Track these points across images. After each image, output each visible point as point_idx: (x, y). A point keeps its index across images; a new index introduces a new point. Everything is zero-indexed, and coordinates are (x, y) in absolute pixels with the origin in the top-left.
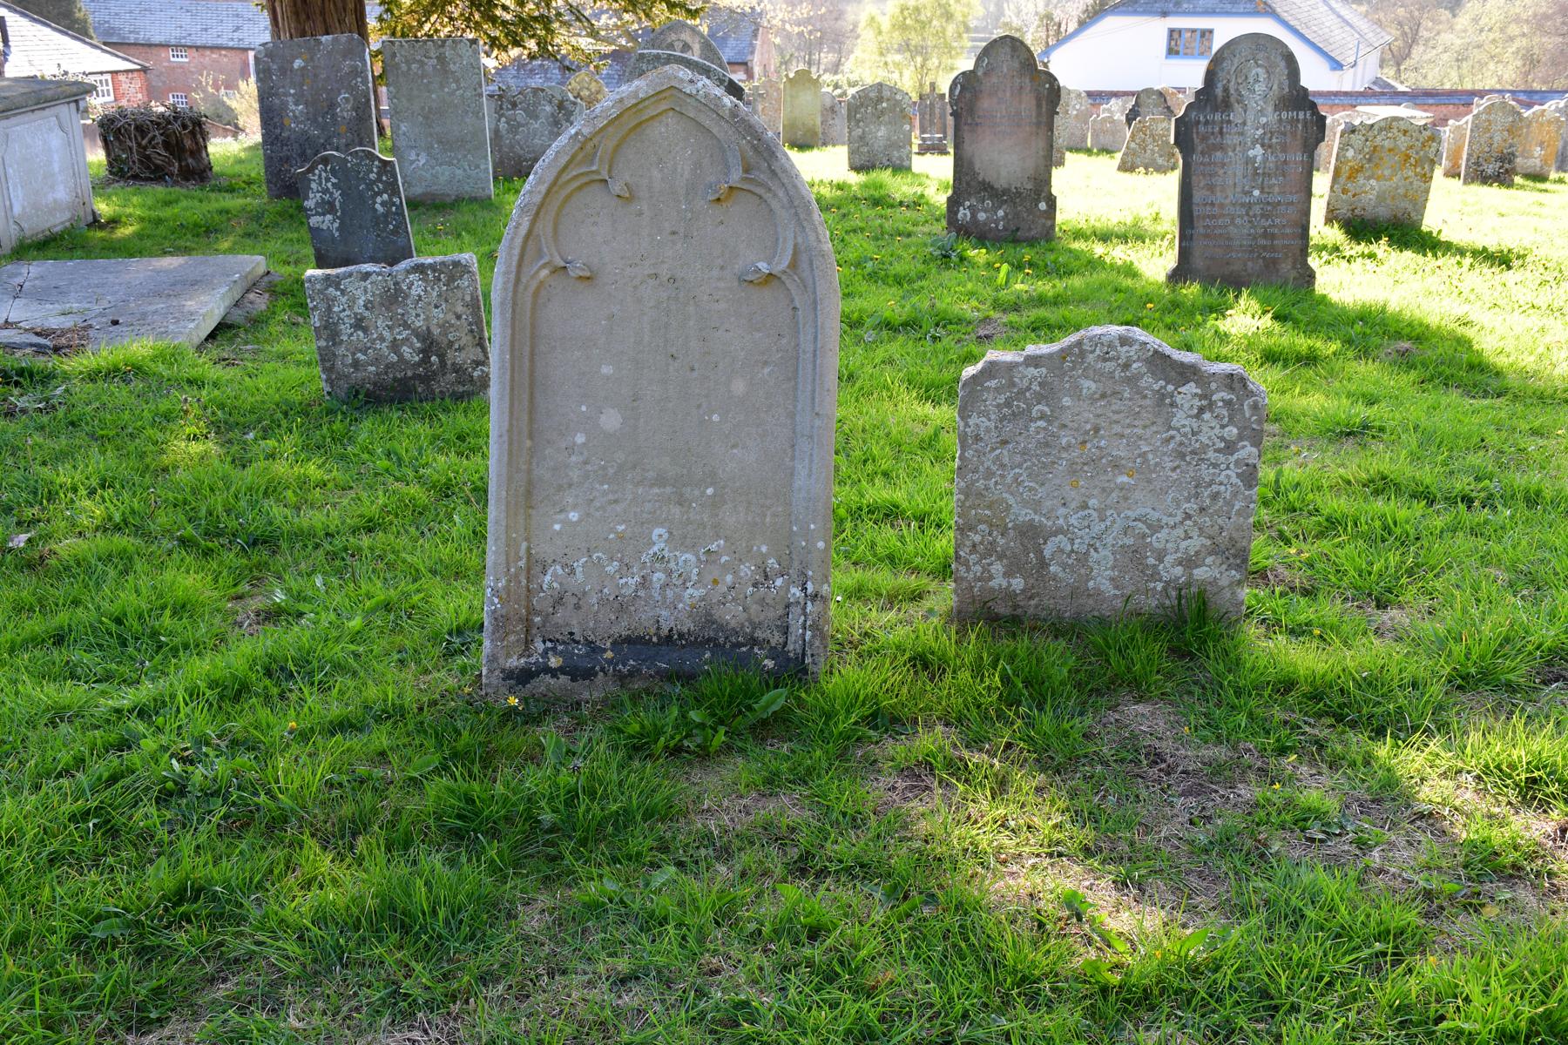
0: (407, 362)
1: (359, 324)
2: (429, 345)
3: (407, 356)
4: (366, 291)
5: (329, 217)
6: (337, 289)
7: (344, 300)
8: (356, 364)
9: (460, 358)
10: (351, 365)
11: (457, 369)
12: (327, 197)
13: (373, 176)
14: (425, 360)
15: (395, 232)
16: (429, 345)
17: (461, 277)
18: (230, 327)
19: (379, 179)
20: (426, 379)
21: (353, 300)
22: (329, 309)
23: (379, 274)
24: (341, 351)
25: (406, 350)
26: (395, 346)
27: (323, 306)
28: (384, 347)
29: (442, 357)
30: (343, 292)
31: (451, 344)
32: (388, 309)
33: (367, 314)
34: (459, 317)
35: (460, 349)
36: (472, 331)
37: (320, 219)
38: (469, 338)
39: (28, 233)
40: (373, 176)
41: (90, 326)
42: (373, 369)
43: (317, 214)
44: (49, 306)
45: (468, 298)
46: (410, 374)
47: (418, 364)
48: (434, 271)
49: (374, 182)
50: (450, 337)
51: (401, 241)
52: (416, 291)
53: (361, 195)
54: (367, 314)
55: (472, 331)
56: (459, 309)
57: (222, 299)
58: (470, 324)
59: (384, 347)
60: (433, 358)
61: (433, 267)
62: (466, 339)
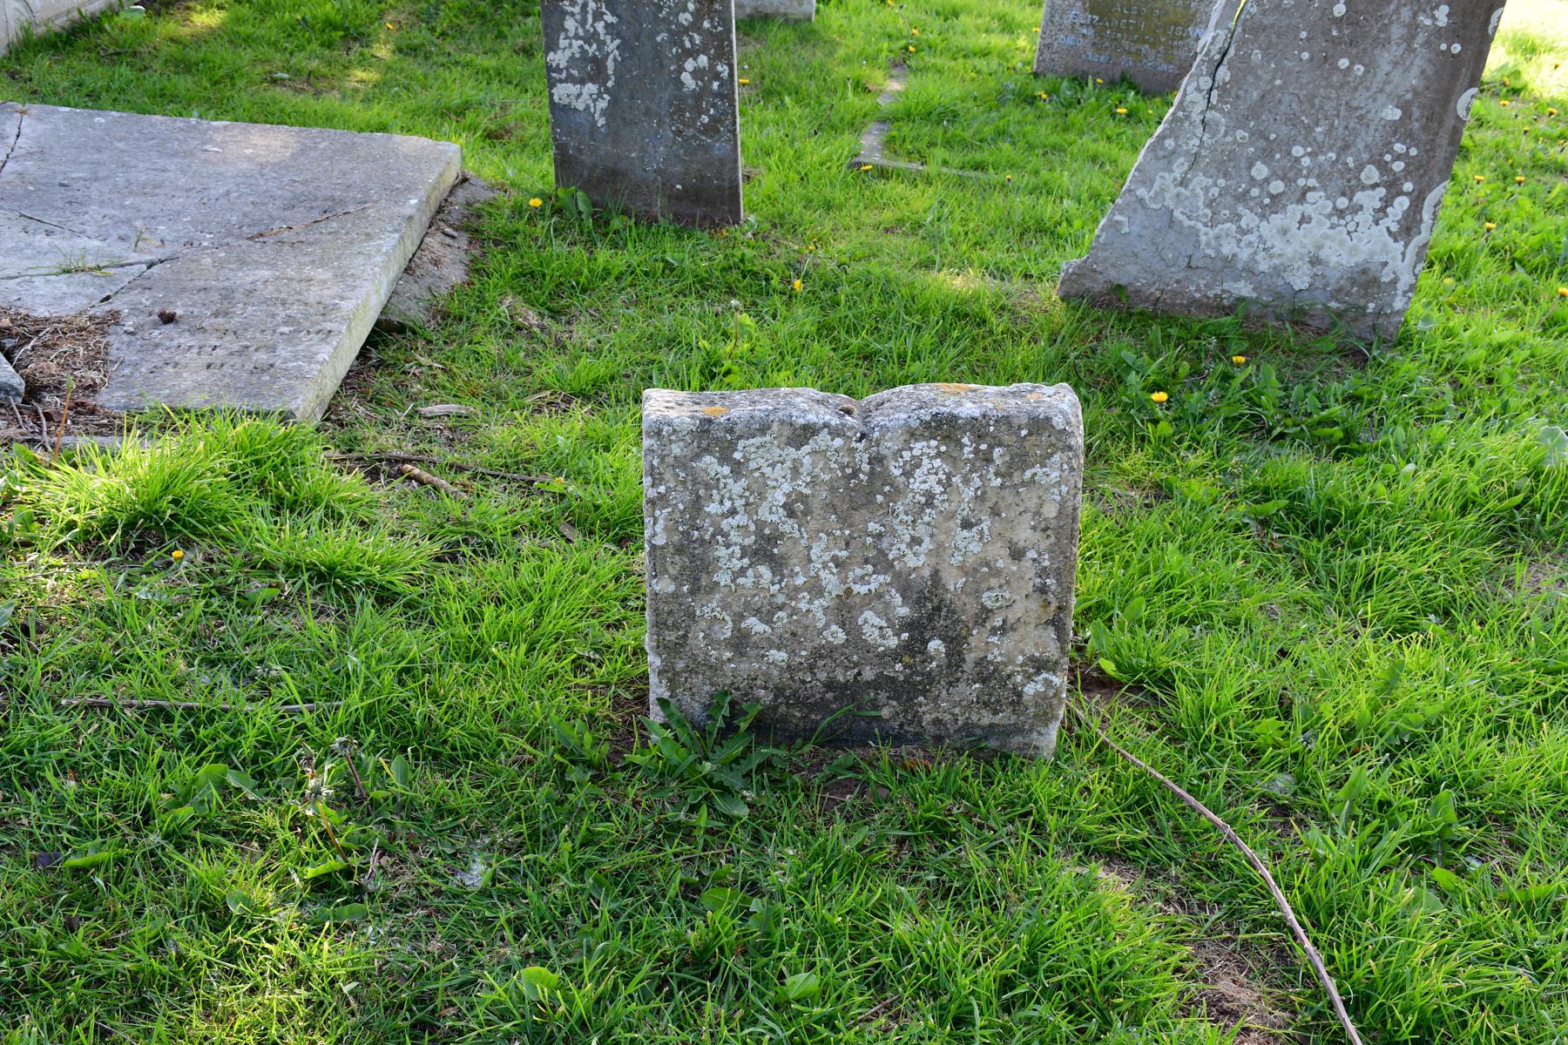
0: (867, 648)
1: (765, 549)
2: (931, 610)
3: (871, 634)
4: (795, 471)
5: (591, 88)
6: (724, 458)
7: (736, 487)
8: (740, 642)
9: (999, 650)
10: (729, 644)
11: (987, 674)
12: (592, 49)
13: (685, 18)
14: (914, 647)
15: (711, 129)
16: (931, 610)
17: (1044, 460)
18: (401, 329)
19: (696, 26)
20: (905, 691)
21: (760, 491)
22: (696, 505)
23: (835, 432)
24: (709, 607)
25: (870, 622)
26: (845, 610)
27: (681, 499)
28: (817, 609)
29: (955, 645)
30: (738, 469)
31: (985, 614)
32: (844, 521)
33: (789, 526)
34: (1017, 554)
35: (1003, 630)
36: (1043, 590)
37: (573, 89)
38: (1034, 604)
39: (40, 16)
40: (685, 18)
41: (115, 318)
42: (779, 656)
43: (570, 79)
44: (42, 241)
45: (1050, 511)
46: (869, 674)
47: (896, 655)
48: (980, 437)
49: (686, 30)
50: (987, 599)
51: (719, 148)
52: (924, 481)
53: (657, 52)
54: (789, 526)
55: (1043, 590)
56: (1024, 534)
57: (385, 268)
58: (1044, 572)
59: (817, 609)
60: (935, 645)
61: (977, 427)
62: (1025, 607)
